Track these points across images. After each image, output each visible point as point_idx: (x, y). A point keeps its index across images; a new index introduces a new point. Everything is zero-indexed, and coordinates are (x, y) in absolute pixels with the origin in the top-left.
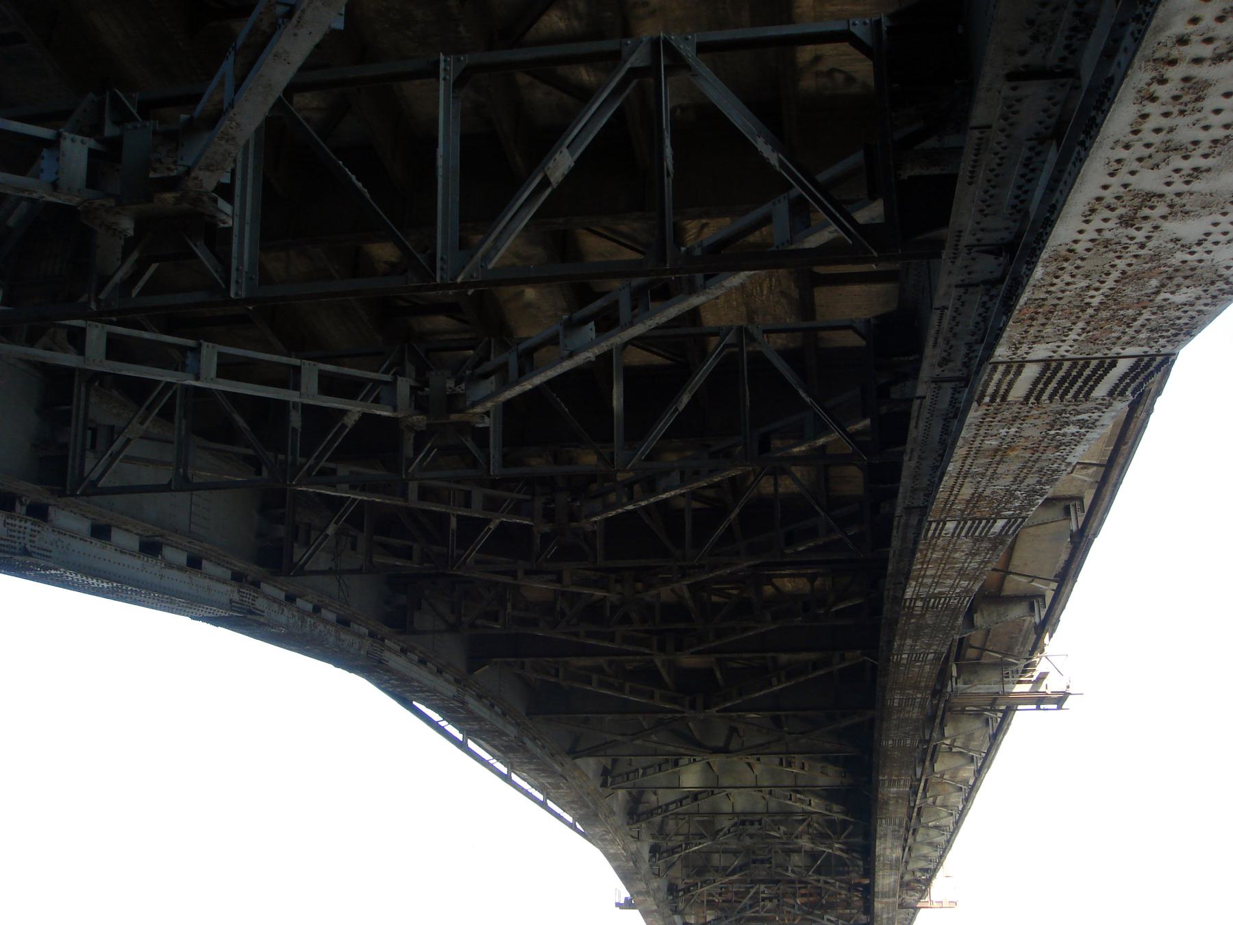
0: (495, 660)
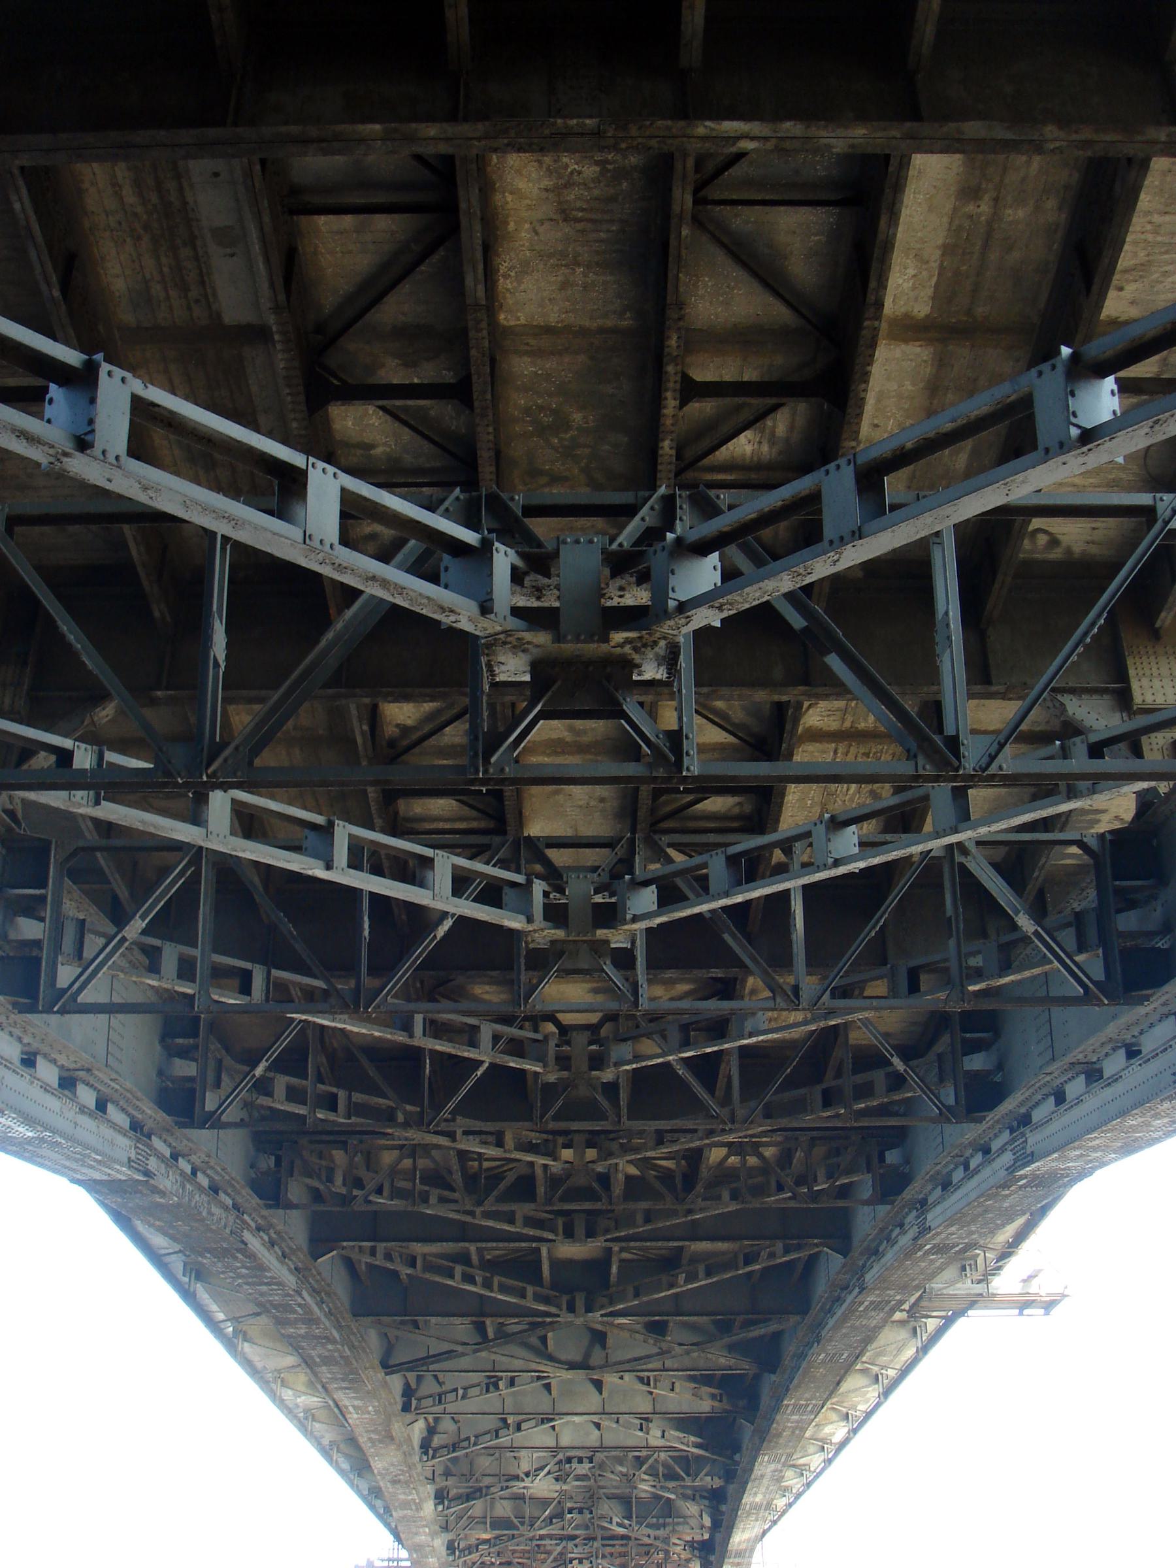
0: (345, 1244)
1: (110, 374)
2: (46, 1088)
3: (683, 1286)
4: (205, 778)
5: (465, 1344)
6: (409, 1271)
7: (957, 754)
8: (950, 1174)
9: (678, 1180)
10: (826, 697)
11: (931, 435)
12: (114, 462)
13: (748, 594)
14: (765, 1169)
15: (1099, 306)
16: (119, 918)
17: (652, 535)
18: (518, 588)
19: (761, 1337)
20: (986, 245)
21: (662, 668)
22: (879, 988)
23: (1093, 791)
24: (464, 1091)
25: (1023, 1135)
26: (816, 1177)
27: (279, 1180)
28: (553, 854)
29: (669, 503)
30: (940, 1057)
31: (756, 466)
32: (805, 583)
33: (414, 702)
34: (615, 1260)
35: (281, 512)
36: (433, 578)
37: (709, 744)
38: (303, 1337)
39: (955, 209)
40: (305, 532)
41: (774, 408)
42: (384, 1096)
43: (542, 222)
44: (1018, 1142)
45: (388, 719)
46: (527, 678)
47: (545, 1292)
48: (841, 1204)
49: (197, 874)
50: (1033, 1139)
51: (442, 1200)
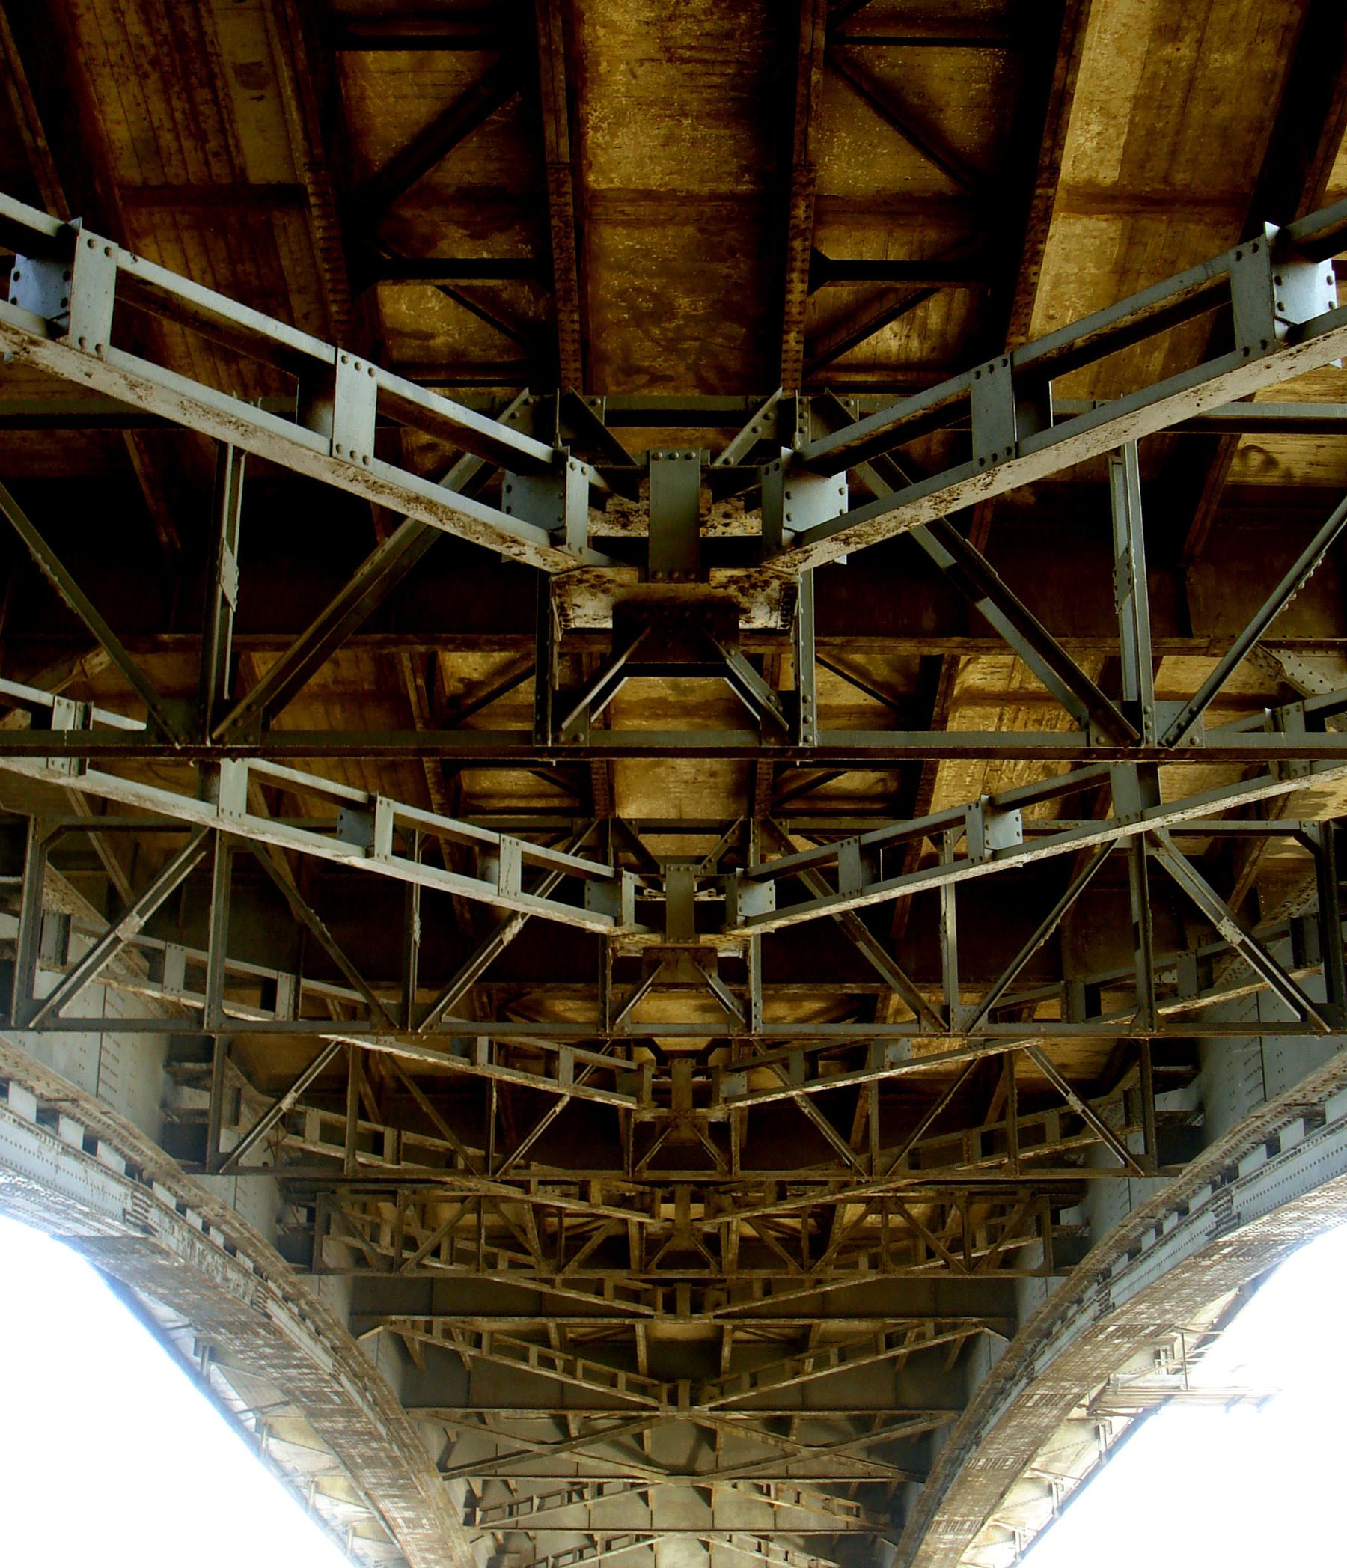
0: (393, 1318)
1: (90, 243)
2: (20, 1122)
3: (811, 1374)
4: (208, 744)
5: (544, 1443)
6: (473, 1352)
7: (1139, 725)
8: (1139, 1239)
9: (805, 1244)
10: (988, 650)
11: (1107, 330)
12: (94, 352)
13: (880, 524)
14: (912, 1230)
15: (1325, 174)
16: (114, 910)
17: (765, 450)
18: (599, 513)
19: (909, 1437)
20: (1187, 98)
21: (775, 614)
22: (1050, 1009)
23: (1311, 771)
24: (539, 1130)
25: (1228, 1192)
26: (974, 1240)
27: (312, 1238)
28: (649, 841)
29: (786, 409)
30: (1127, 1095)
31: (905, 366)
32: (950, 511)
33: (481, 650)
34: (726, 1340)
35: (305, 418)
36: (493, 500)
37: (845, 706)
38: (340, 1432)
39: (1148, 52)
40: (331, 441)
41: (924, 295)
42: (442, 1137)
43: (641, 62)
44: (1222, 1202)
45: (450, 670)
46: (609, 624)
47: (640, 1379)
48: (1004, 1274)
49: (209, 860)
50: (1241, 1198)
51: (514, 1265)
